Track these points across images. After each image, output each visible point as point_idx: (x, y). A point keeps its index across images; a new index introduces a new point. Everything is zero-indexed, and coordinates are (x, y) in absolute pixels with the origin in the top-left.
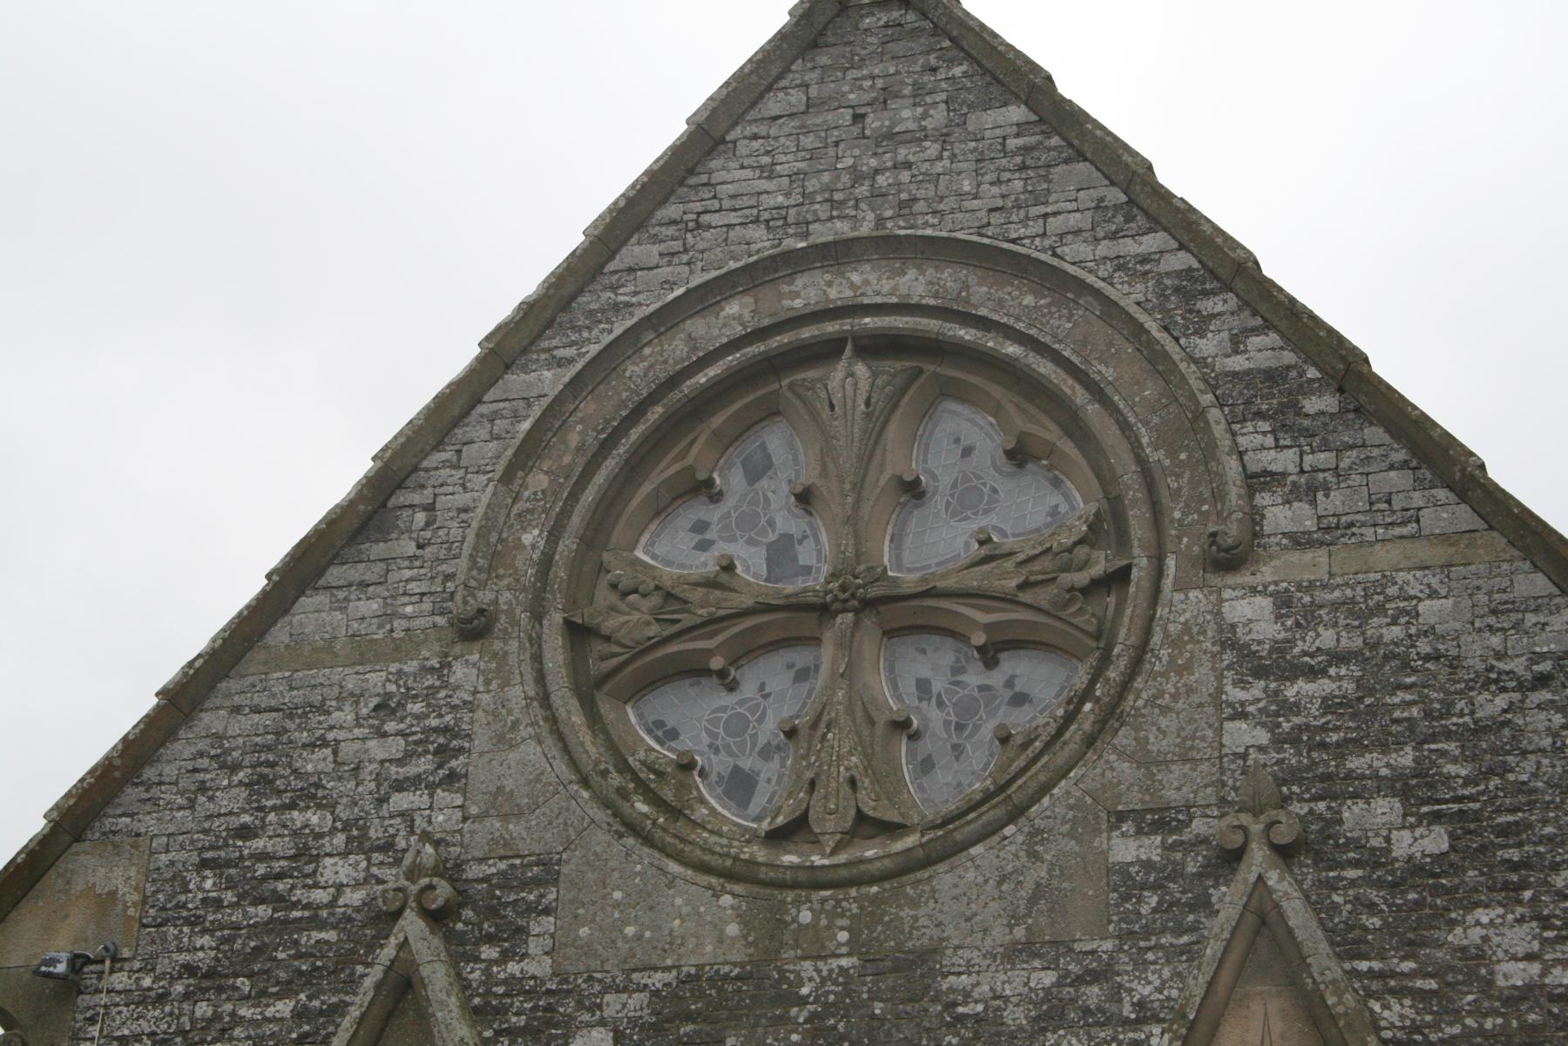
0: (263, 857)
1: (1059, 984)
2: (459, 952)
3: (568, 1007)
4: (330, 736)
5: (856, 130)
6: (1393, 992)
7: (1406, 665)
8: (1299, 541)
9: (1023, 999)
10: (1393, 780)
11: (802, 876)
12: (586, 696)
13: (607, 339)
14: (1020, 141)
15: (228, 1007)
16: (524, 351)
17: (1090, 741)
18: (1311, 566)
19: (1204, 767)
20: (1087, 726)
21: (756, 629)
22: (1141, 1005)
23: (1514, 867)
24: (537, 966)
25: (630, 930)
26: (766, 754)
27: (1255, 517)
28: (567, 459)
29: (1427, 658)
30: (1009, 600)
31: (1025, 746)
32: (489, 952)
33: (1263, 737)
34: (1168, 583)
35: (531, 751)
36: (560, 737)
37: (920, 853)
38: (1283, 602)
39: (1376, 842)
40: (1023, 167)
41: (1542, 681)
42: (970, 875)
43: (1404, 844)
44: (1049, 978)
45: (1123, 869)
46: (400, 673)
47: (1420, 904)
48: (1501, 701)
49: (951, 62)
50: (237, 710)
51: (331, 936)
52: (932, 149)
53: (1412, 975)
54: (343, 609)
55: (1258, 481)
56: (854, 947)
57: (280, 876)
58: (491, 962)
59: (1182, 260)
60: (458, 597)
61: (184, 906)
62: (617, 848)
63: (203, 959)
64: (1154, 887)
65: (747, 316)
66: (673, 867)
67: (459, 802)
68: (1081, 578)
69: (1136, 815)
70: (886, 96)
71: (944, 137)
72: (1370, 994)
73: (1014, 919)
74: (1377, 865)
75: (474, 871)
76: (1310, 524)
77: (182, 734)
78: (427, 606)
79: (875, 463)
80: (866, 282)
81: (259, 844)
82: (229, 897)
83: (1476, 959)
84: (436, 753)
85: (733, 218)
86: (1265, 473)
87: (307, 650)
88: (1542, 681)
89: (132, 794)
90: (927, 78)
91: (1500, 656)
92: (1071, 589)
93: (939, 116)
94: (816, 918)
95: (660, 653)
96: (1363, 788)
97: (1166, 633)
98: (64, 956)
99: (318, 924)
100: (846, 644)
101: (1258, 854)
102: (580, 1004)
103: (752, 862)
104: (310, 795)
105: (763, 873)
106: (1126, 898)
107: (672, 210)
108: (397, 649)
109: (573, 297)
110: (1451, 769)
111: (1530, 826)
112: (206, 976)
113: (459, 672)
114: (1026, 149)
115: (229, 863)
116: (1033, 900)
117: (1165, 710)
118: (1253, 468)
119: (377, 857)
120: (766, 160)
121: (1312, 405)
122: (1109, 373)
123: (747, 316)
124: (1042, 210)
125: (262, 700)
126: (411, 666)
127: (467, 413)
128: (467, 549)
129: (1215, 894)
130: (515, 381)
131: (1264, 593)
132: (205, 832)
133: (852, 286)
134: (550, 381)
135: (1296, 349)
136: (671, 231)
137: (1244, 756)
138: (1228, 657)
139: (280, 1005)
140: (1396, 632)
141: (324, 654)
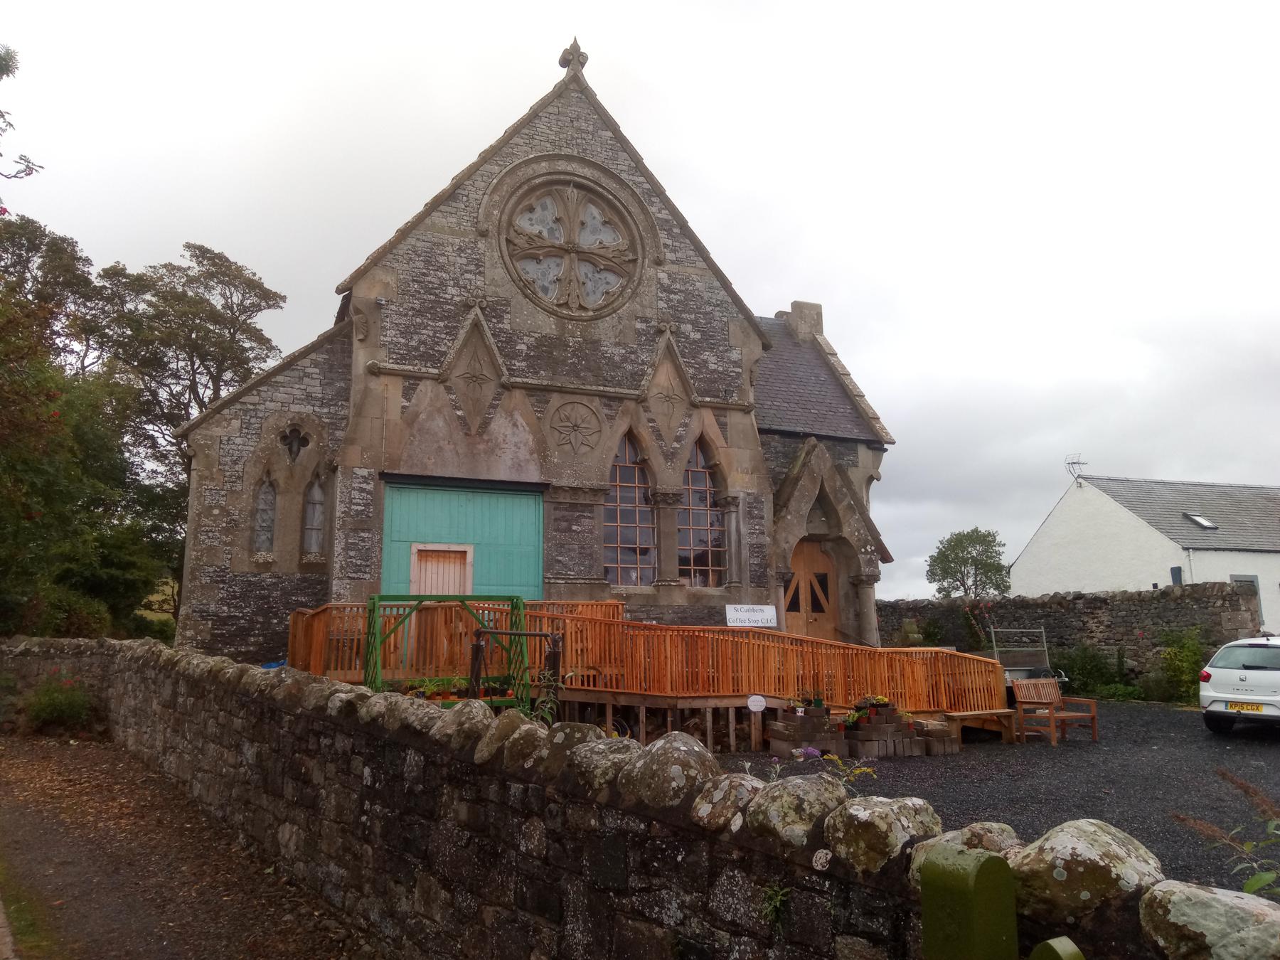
0: (430, 282)
8: (673, 262)
11: (568, 317)
12: (511, 256)
18: (675, 268)
21: (549, 251)
22: (642, 361)
30: (609, 259)
36: (507, 269)
38: (670, 276)
41: (718, 305)
44: (624, 351)
48: (711, 308)
50: (418, 239)
51: (452, 308)
55: (666, 246)
57: (436, 289)
59: (647, 186)
63: (417, 306)
64: (645, 335)
68: (627, 259)
70: (578, 118)
81: (429, 279)
82: (422, 291)
83: (706, 362)
88: (718, 305)
100: (571, 261)
104: (441, 268)
113: (480, 245)
114: (611, 145)
115: (421, 282)
116: (620, 333)
119: (463, 290)
136: (526, 137)
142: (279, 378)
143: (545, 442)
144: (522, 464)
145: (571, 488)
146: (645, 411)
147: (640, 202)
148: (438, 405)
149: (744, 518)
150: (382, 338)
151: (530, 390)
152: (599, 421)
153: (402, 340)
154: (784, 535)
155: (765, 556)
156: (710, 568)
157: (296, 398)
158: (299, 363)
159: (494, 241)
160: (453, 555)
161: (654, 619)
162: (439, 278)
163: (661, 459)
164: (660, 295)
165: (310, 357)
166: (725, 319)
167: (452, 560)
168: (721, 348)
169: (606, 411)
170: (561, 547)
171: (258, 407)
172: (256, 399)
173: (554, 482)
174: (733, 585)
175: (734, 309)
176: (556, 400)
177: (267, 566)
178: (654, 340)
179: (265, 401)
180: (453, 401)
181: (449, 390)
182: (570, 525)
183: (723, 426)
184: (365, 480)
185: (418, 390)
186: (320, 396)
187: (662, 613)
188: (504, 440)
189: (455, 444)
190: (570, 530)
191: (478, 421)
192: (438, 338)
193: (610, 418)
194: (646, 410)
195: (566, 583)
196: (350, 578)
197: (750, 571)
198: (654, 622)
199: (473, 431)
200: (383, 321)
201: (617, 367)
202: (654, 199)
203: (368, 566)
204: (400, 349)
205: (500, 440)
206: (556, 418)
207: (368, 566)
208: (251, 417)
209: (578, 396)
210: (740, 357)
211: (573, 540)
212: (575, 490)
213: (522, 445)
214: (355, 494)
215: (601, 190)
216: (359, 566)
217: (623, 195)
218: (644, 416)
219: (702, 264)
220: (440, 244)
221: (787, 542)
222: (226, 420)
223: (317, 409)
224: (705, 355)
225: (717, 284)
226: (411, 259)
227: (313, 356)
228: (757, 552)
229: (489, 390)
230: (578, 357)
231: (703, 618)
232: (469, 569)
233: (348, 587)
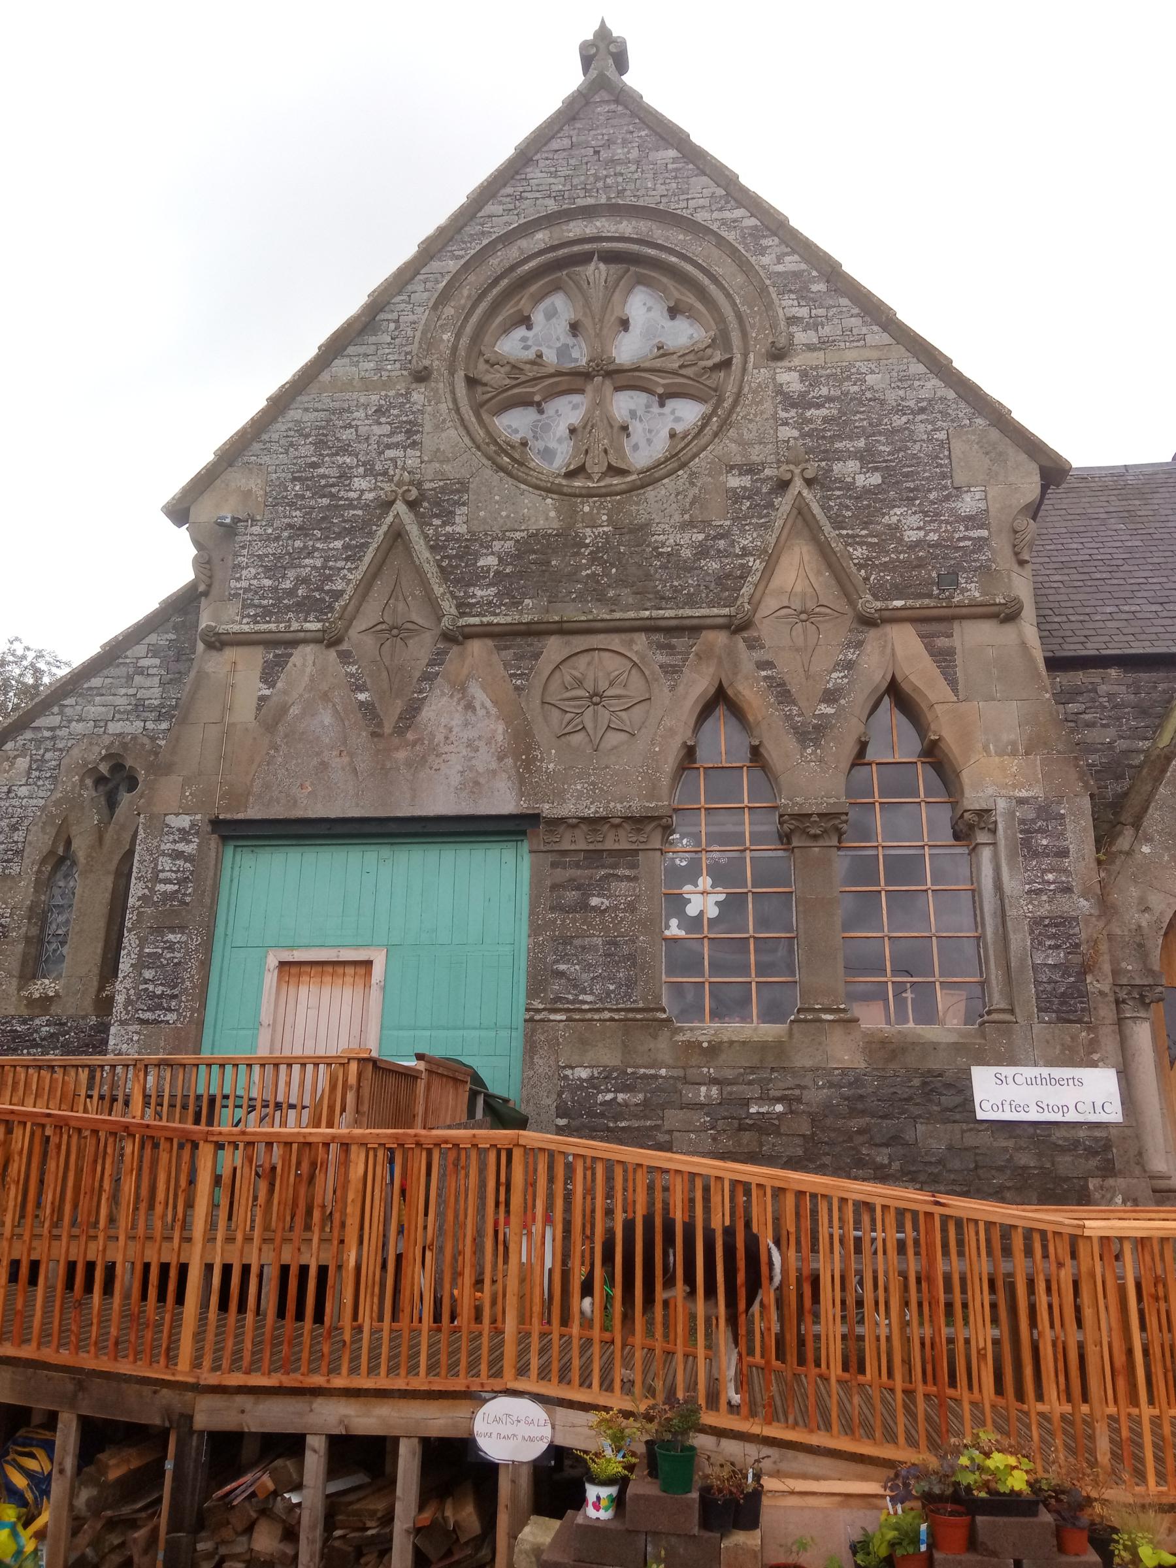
0: (324, 476)
1: (706, 539)
2: (422, 521)
3: (476, 546)
4: (353, 423)
5: (596, 157)
6: (858, 543)
7: (861, 403)
8: (810, 348)
9: (689, 546)
10: (856, 453)
11: (584, 492)
12: (477, 408)
13: (478, 248)
14: (675, 166)
15: (311, 543)
16: (440, 251)
17: (716, 435)
18: (816, 358)
19: (770, 446)
20: (715, 428)
21: (557, 383)
22: (743, 548)
23: (912, 490)
24: (461, 529)
25: (504, 514)
26: (560, 441)
27: (791, 336)
28: (463, 301)
29: (870, 400)
30: (674, 373)
31: (683, 438)
32: (437, 522)
33: (796, 433)
34: (750, 365)
35: (452, 433)
36: (466, 428)
37: (639, 483)
38: (804, 375)
39: (849, 480)
40: (676, 178)
41: (922, 410)
42: (663, 492)
43: (861, 480)
44: (701, 537)
45: (734, 490)
46: (386, 396)
47: (869, 506)
48: (904, 419)
49: (640, 130)
50: (306, 410)
51: (360, 512)
52: (633, 168)
53: (866, 536)
54: (357, 366)
55: (792, 320)
56: (610, 522)
57: (333, 485)
58: (437, 526)
59: (753, 222)
60: (414, 361)
61: (286, 497)
62: (496, 477)
63: (298, 521)
64: (748, 498)
65: (547, 240)
66: (523, 486)
67: (418, 454)
68: (710, 363)
69: (739, 467)
70: (609, 143)
71: (638, 163)
72: (850, 545)
73: (684, 512)
74: (849, 489)
75: (427, 486)
76: (815, 340)
77: (280, 419)
78: (398, 365)
79: (609, 310)
80: (603, 226)
81: (321, 471)
82: (308, 494)
83: (896, 528)
84: (406, 432)
85: (538, 195)
86: (794, 317)
87: (340, 383)
88: (922, 410)
89: (257, 446)
90: (629, 136)
91: (902, 399)
92: (704, 368)
93: (635, 154)
94: (591, 510)
95: (510, 393)
96: (841, 456)
97: (750, 388)
98: (229, 516)
99: (351, 506)
100: (598, 390)
101: (798, 485)
102: (481, 546)
103: (560, 485)
104: (345, 449)
105: (565, 490)
106: (735, 503)
107: (509, 190)
108: (384, 385)
109: (462, 228)
110: (882, 448)
111: (918, 473)
112: (298, 529)
113: (415, 396)
114: (676, 170)
115: (307, 479)
116: (692, 504)
117: (751, 421)
118: (789, 315)
119: (380, 478)
120: (553, 169)
121: (815, 288)
122: (721, 271)
123: (547, 240)
124: (686, 197)
125: (319, 406)
126: (392, 393)
127: (412, 279)
128: (417, 339)
129: (776, 501)
130: (435, 265)
131: (795, 370)
132: (294, 464)
133: (597, 228)
134: (453, 266)
135: (807, 262)
136: (508, 199)
137: (788, 442)
138: (779, 398)
139: (336, 543)
140: (856, 388)
141: (348, 386)
142: (96, 682)
143: (529, 733)
144: (482, 780)
145: (584, 820)
146: (751, 647)
147: (733, 252)
148: (324, 687)
149: (1012, 857)
150: (233, 584)
151: (501, 636)
152: (647, 681)
153: (267, 582)
154: (1134, 892)
155: (1077, 946)
156: (937, 977)
157: (119, 712)
158: (129, 653)
159: (441, 385)
160: (350, 970)
161: (779, 1100)
162: (339, 466)
163: (791, 743)
164: (783, 415)
165: (147, 641)
166: (942, 435)
167: (349, 979)
168: (933, 496)
169: (662, 658)
170: (565, 943)
171: (58, 732)
172: (55, 720)
173: (546, 809)
174: (995, 1017)
175: (963, 410)
176: (554, 648)
177: (45, 1002)
178: (771, 505)
179: (70, 721)
180: (352, 675)
181: (345, 657)
182: (587, 896)
183: (944, 658)
184: (184, 835)
185: (290, 664)
186: (156, 702)
187: (798, 1086)
188: (447, 738)
189: (351, 755)
190: (584, 907)
191: (399, 705)
192: (330, 568)
193: (671, 670)
194: (753, 644)
195: (569, 1020)
196: (143, 1022)
197: (1037, 983)
198: (779, 1108)
199: (388, 729)
200: (236, 555)
201: (687, 568)
202: (765, 242)
203: (174, 997)
204: (263, 598)
205: (439, 738)
206: (555, 684)
207: (174, 997)
208: (47, 750)
209: (601, 637)
210: (982, 505)
211: (590, 925)
212: (594, 823)
213: (482, 744)
214: (165, 863)
215: (674, 259)
216: (160, 997)
217: (699, 249)
218: (747, 659)
219: (878, 337)
220: (343, 410)
221: (1147, 909)
222: (8, 759)
223: (150, 725)
224: (894, 515)
225: (918, 368)
226: (291, 445)
227: (153, 638)
228: (1053, 937)
229: (420, 649)
230: (603, 563)
231: (908, 1099)
232: (375, 994)
233: (136, 1038)
